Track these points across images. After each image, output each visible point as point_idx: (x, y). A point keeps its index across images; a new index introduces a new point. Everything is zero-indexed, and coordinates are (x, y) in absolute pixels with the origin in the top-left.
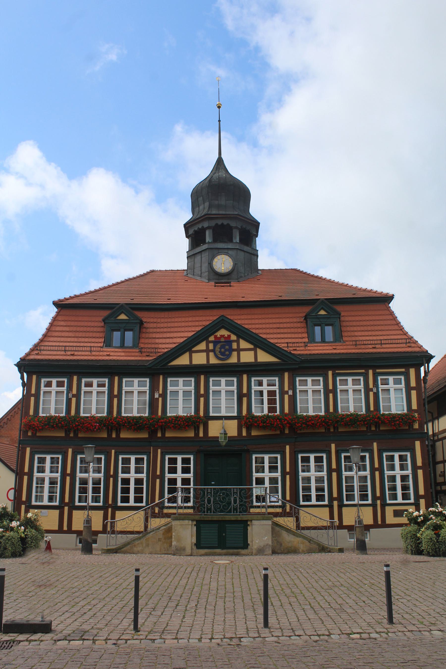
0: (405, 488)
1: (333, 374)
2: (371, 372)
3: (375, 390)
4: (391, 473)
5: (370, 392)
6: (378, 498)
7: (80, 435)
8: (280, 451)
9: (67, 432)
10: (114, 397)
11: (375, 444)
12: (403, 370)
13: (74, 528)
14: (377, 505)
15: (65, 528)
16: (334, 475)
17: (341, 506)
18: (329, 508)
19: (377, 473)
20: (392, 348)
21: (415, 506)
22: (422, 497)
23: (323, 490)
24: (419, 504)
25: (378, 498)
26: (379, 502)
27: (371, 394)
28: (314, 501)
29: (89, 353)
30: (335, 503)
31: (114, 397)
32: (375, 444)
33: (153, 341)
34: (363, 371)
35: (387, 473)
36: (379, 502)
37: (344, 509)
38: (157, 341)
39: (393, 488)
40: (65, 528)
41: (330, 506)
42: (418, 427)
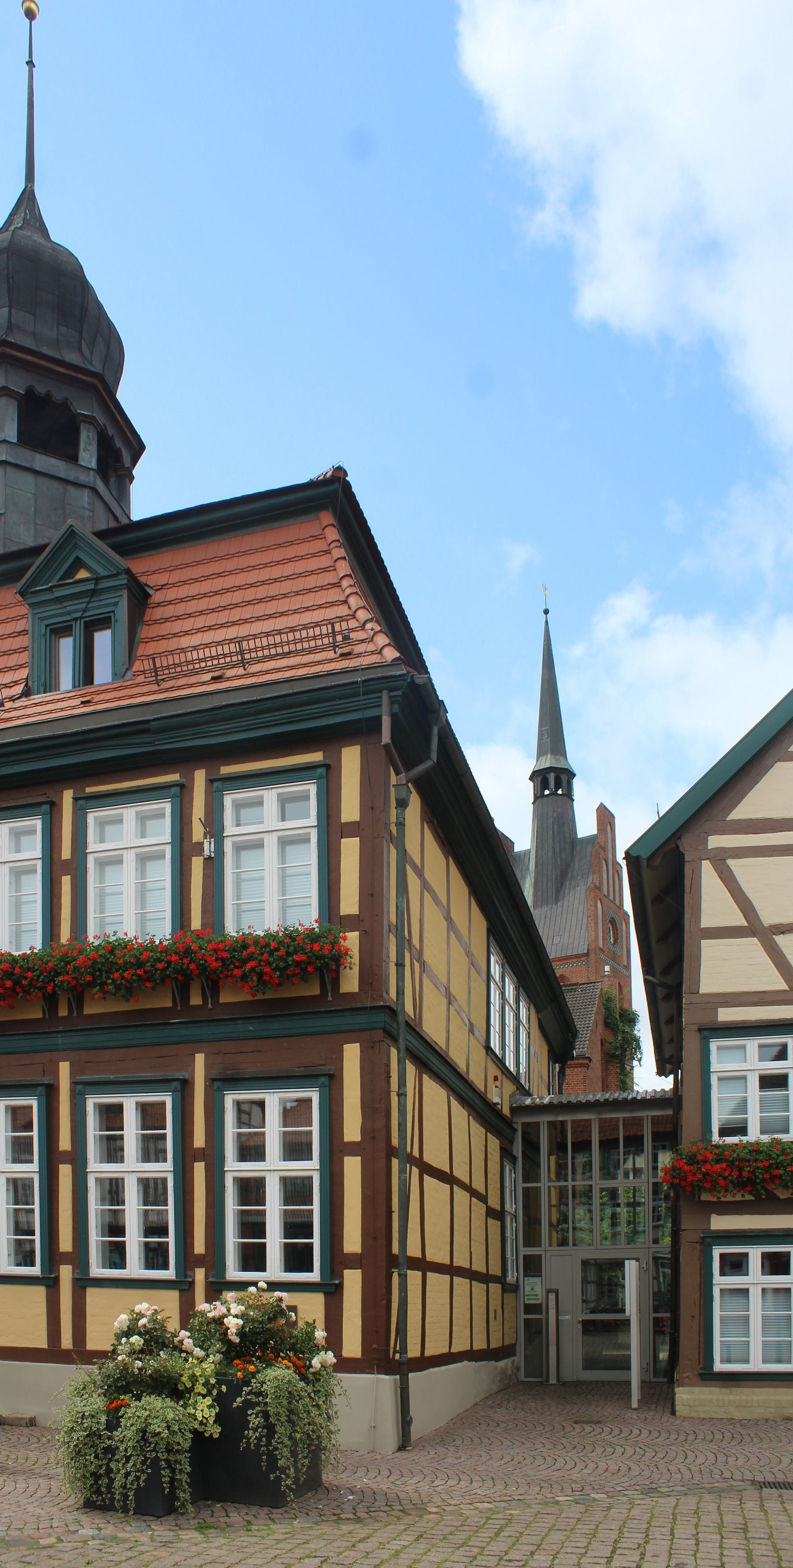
0: (297, 1227)
1: (210, 781)
2: (200, 777)
3: (208, 848)
4: (111, 1169)
5: (194, 859)
6: (67, 1258)
7: (89, 1010)
8: (318, 1076)
9: (51, 1002)
10: (196, 861)
11: (200, 1059)
12: (317, 757)
13: (92, 1344)
14: (192, 1284)
15: (67, 1342)
16: (65, 1172)
17: (83, 1283)
18: (48, 1287)
19: (199, 1169)
20: (305, 665)
21: (326, 1294)
22: (353, 1261)
23: (163, 1231)
24: (340, 1287)
25: (200, 1261)
26: (200, 1275)
27: (197, 865)
28: (135, 1267)
29: (155, 688)
30: (66, 1272)
31: (196, 861)
32: (200, 1059)
33: (173, 644)
34: (175, 777)
35: (235, 1168)
36: (200, 1275)
37: (93, 1295)
38: (185, 642)
39: (253, 1227)
40: (67, 1342)
41: (50, 1282)
42: (356, 989)
